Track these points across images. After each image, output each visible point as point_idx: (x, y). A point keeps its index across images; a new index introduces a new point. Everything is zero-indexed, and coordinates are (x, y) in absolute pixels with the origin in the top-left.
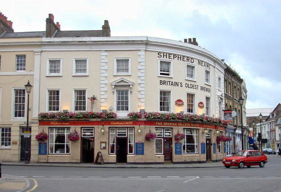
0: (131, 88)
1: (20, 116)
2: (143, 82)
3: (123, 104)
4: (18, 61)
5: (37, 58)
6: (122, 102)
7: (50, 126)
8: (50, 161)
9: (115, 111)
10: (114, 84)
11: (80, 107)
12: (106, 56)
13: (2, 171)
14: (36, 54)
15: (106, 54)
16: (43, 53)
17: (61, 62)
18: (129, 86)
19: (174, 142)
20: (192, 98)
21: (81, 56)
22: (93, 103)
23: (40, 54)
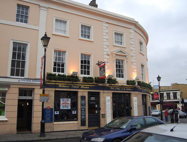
0: (127, 59)
1: (17, 75)
2: (133, 43)
3: (120, 74)
4: (18, 12)
5: (43, 13)
6: (119, 70)
7: (57, 89)
8: (54, 131)
9: (115, 77)
10: (115, 53)
11: (85, 71)
12: (107, 27)
13: (40, 131)
14: (41, 8)
15: (107, 25)
16: (50, 9)
17: (124, 36)
18: (125, 56)
19: (125, 57)
20: (146, 98)
21: (87, 23)
22: (45, 46)
23: (46, 9)
